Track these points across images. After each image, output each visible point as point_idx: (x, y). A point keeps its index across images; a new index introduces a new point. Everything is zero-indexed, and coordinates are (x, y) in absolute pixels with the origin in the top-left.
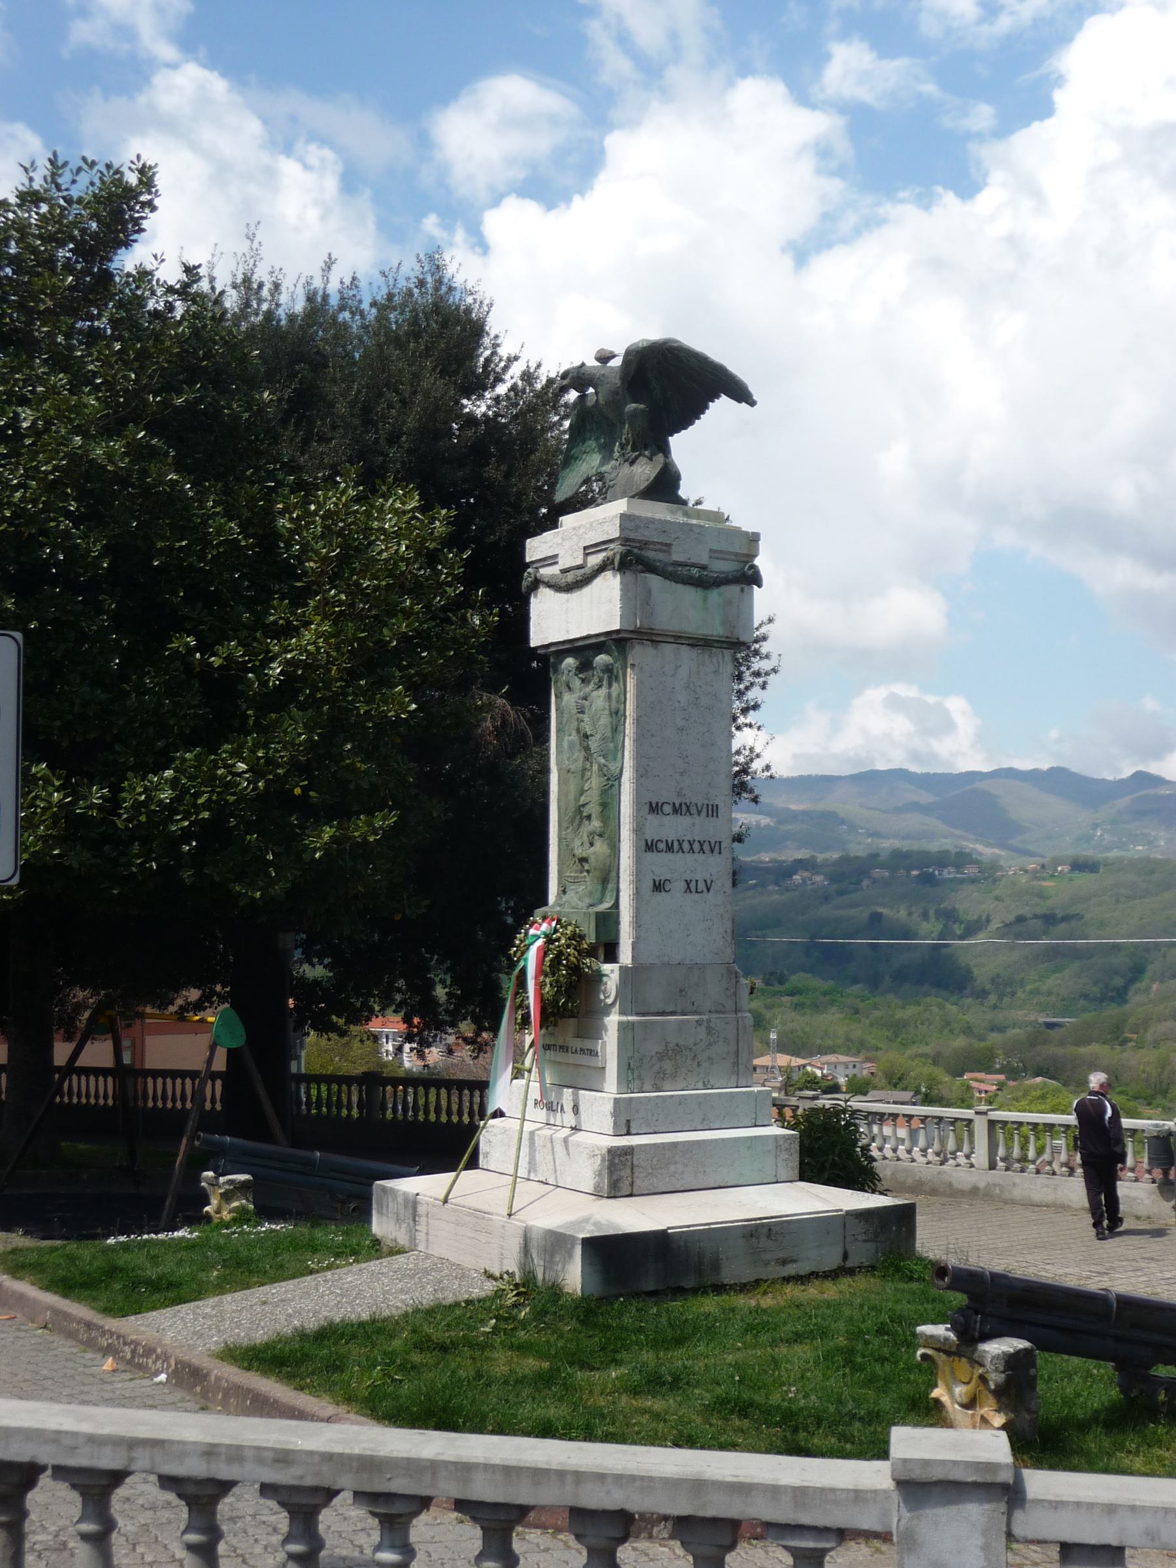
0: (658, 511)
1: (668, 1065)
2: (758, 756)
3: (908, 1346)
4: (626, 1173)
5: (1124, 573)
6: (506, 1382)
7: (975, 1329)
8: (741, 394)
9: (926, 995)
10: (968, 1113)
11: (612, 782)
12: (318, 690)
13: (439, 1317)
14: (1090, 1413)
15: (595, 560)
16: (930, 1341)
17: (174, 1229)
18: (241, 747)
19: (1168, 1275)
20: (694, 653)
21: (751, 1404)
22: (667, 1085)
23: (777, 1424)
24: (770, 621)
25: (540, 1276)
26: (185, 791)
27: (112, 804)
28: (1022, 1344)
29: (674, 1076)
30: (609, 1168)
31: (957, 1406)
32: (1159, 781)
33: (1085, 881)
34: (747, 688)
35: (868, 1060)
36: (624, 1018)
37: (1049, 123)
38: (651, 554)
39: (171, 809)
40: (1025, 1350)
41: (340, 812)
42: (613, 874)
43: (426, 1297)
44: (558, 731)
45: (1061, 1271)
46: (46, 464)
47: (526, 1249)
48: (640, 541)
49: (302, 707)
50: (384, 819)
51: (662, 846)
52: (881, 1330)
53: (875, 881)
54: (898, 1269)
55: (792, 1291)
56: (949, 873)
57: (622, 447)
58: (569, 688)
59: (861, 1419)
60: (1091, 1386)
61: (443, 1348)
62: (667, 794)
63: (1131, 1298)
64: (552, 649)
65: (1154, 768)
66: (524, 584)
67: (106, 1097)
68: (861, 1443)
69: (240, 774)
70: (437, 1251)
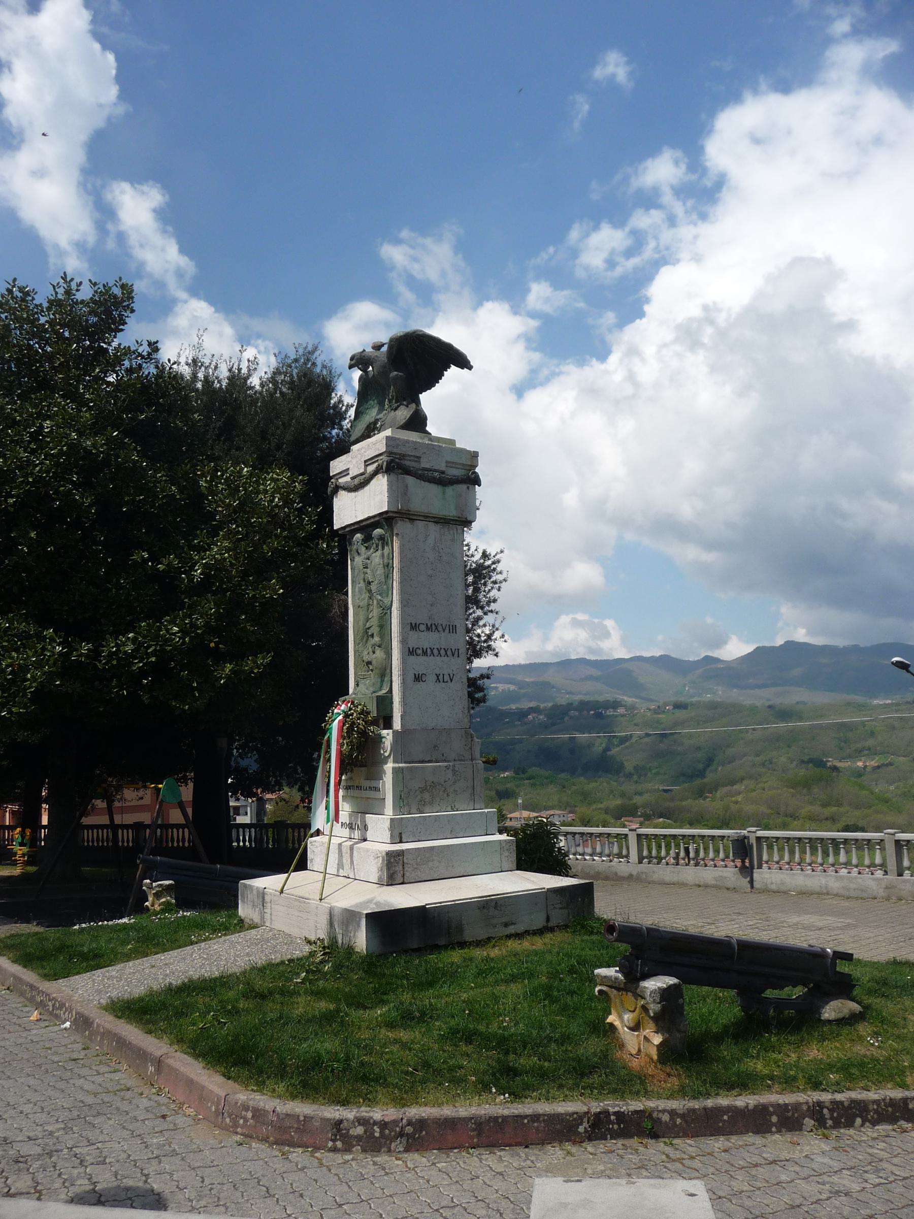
0: (413, 436)
1: (427, 796)
2: (497, 629)
3: (590, 982)
4: (399, 868)
5: (691, 553)
6: (299, 1022)
8: (463, 362)
9: (600, 777)
10: (625, 831)
11: (386, 611)
12: (225, 583)
13: (268, 972)
15: (371, 468)
16: (605, 980)
17: (121, 918)
18: (175, 618)
19: (751, 923)
20: (439, 526)
21: (475, 1032)
22: (426, 809)
23: (493, 1048)
24: (502, 552)
25: (340, 941)
26: (140, 645)
27: (95, 654)
28: (672, 981)
29: (431, 803)
30: (387, 865)
32: (717, 660)
33: (681, 714)
34: (489, 591)
35: (571, 812)
36: (397, 765)
37: (644, 320)
38: (407, 463)
39: (133, 655)
40: (675, 985)
41: (237, 656)
42: (388, 671)
43: (260, 959)
44: (353, 582)
45: (685, 923)
46: (54, 449)
47: (331, 923)
48: (400, 454)
49: (214, 593)
50: (263, 659)
51: (419, 652)
52: (572, 971)
53: (571, 718)
54: (583, 927)
55: (513, 945)
56: (610, 712)
57: (390, 401)
58: (359, 554)
59: (556, 1041)
61: (263, 997)
62: (422, 618)
63: (748, 942)
64: (348, 529)
65: (715, 654)
66: (329, 490)
67: (128, 841)
68: (556, 1061)
69: (174, 634)
70: (277, 926)
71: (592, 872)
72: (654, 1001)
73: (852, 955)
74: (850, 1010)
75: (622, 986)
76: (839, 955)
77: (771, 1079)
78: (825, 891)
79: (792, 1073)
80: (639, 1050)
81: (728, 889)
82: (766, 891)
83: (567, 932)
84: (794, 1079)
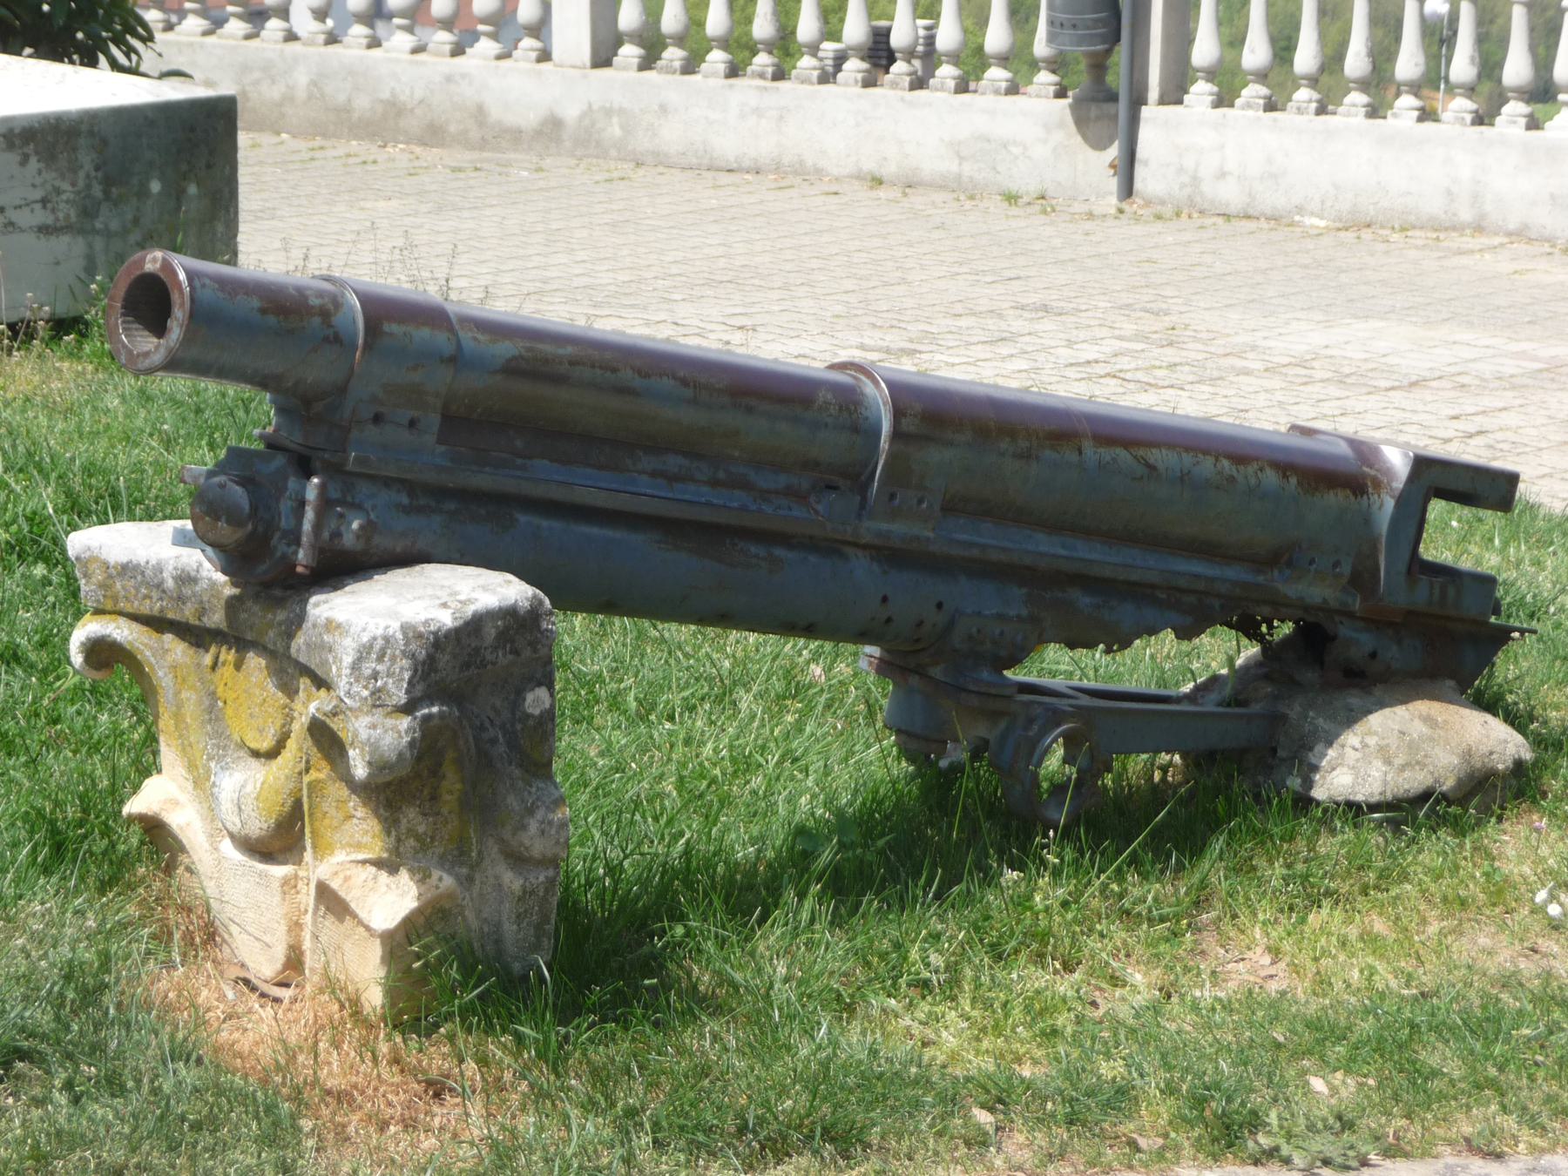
7: (295, 538)
14: (779, 837)
19: (1090, 353)
28: (494, 590)
31: (227, 846)
40: (509, 614)
60: (799, 727)
71: (362, 103)
72: (377, 700)
73: (1512, 479)
74: (1468, 754)
75: (216, 619)
76: (1441, 479)
77: (998, 1101)
78: (1466, 215)
79: (1110, 1070)
80: (294, 962)
81: (1011, 198)
82: (1188, 209)
83: (74, 354)
84: (1122, 1098)
